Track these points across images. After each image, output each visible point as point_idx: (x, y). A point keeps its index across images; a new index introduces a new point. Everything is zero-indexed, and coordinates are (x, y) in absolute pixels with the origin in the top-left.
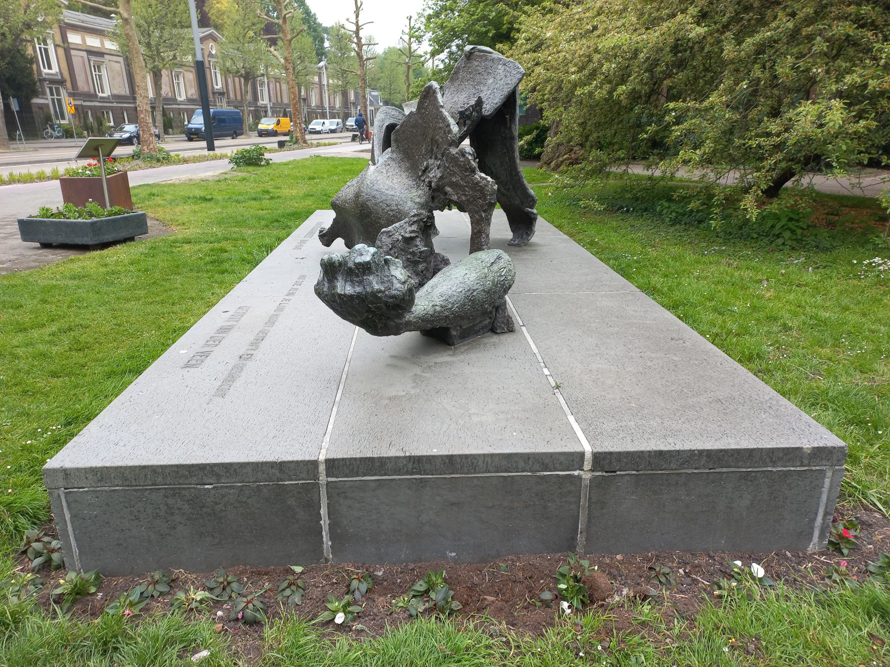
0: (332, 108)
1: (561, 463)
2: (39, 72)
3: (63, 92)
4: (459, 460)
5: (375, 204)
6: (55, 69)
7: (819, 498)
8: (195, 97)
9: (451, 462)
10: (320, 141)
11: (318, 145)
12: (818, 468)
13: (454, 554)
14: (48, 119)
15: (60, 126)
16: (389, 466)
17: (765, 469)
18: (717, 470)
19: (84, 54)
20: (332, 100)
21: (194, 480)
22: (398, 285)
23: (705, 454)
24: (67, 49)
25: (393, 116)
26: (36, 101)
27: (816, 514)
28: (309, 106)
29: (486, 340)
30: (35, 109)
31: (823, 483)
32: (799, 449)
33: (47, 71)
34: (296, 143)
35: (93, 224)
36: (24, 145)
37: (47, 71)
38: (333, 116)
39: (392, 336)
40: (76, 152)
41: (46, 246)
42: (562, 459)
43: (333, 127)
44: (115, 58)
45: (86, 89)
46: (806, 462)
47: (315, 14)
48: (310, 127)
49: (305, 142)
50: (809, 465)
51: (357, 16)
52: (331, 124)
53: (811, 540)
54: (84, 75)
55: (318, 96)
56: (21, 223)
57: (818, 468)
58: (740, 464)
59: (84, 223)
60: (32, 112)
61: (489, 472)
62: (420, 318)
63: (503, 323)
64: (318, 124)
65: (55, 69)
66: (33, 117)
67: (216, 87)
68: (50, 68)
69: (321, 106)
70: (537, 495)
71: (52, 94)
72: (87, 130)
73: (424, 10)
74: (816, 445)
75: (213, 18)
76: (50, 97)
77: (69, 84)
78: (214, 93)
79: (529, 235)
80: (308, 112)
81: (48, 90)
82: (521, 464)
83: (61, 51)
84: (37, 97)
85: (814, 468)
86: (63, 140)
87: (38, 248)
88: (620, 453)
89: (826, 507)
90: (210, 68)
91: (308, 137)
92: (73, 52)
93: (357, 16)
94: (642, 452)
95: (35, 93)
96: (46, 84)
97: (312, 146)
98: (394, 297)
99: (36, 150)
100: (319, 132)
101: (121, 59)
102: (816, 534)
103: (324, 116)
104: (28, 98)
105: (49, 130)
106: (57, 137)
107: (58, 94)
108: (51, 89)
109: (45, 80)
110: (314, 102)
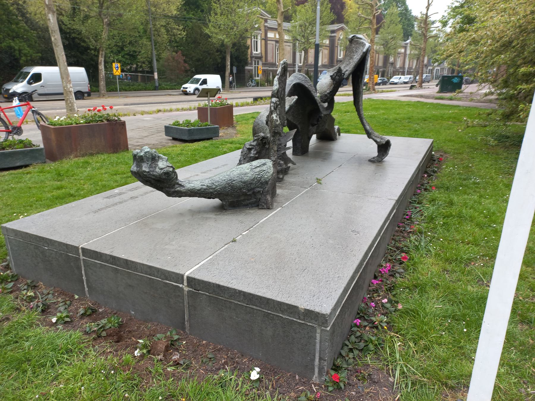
0: (409, 68)
1: (173, 278)
2: (251, 53)
3: (260, 63)
4: (130, 263)
5: (259, 128)
6: (259, 51)
7: (315, 345)
8: (326, 64)
9: (127, 263)
10: (384, 90)
11: (382, 92)
12: (311, 324)
13: (133, 313)
14: (251, 77)
15: (255, 80)
16: (104, 258)
17: (279, 314)
18: (251, 306)
19: (274, 43)
20: (411, 63)
21: (41, 243)
22: (157, 170)
23: (242, 293)
24: (266, 39)
25: (299, 79)
26: (247, 68)
27: (314, 356)
28: (395, 67)
29: (247, 211)
30: (246, 72)
31: (316, 337)
32: (296, 307)
33: (255, 52)
34: (368, 90)
35: (189, 130)
36: (236, 90)
37: (255, 52)
38: (409, 73)
39: (197, 198)
40: (269, 94)
41: (174, 139)
42: (173, 275)
43: (406, 81)
44: (288, 44)
45: (271, 61)
46: (302, 317)
47: (411, 10)
48: (391, 80)
49: (374, 90)
50: (304, 320)
51: (428, 10)
52: (405, 78)
53: (313, 373)
54: (272, 54)
55: (402, 61)
56: (166, 128)
57: (311, 324)
58: (263, 306)
59: (194, 129)
60: (245, 74)
61: (143, 273)
62: (189, 190)
63: (264, 203)
64: (396, 78)
65: (259, 51)
66: (244, 76)
67: (339, 57)
68: (257, 51)
69: (403, 67)
70: (164, 292)
71: (255, 64)
72: (267, 82)
73: (453, 3)
74: (308, 308)
75: (347, 18)
76: (254, 66)
77: (264, 59)
78: (337, 61)
79: (383, 156)
80: (393, 71)
81: (254, 62)
82: (156, 274)
83: (263, 42)
84: (247, 66)
85: (309, 324)
86: (256, 87)
87: (170, 140)
88: (199, 280)
89: (320, 354)
90: (337, 47)
91: (376, 87)
92: (269, 42)
93: (428, 10)
94: (210, 283)
95: (246, 64)
96: (253, 59)
97: (378, 92)
98: (154, 175)
99: (240, 92)
100: (396, 84)
101: (291, 44)
102: (316, 370)
103: (403, 74)
104: (243, 67)
105: (250, 83)
106: (253, 86)
107: (258, 64)
108: (255, 61)
109: (253, 57)
110: (398, 65)
